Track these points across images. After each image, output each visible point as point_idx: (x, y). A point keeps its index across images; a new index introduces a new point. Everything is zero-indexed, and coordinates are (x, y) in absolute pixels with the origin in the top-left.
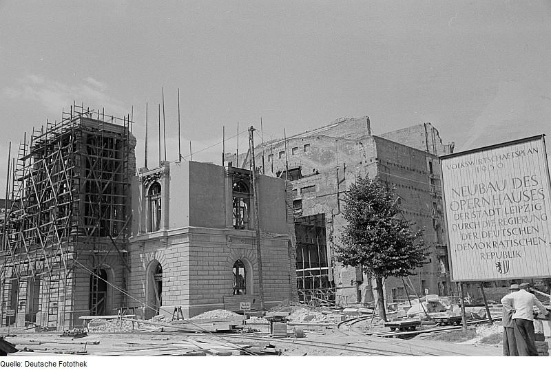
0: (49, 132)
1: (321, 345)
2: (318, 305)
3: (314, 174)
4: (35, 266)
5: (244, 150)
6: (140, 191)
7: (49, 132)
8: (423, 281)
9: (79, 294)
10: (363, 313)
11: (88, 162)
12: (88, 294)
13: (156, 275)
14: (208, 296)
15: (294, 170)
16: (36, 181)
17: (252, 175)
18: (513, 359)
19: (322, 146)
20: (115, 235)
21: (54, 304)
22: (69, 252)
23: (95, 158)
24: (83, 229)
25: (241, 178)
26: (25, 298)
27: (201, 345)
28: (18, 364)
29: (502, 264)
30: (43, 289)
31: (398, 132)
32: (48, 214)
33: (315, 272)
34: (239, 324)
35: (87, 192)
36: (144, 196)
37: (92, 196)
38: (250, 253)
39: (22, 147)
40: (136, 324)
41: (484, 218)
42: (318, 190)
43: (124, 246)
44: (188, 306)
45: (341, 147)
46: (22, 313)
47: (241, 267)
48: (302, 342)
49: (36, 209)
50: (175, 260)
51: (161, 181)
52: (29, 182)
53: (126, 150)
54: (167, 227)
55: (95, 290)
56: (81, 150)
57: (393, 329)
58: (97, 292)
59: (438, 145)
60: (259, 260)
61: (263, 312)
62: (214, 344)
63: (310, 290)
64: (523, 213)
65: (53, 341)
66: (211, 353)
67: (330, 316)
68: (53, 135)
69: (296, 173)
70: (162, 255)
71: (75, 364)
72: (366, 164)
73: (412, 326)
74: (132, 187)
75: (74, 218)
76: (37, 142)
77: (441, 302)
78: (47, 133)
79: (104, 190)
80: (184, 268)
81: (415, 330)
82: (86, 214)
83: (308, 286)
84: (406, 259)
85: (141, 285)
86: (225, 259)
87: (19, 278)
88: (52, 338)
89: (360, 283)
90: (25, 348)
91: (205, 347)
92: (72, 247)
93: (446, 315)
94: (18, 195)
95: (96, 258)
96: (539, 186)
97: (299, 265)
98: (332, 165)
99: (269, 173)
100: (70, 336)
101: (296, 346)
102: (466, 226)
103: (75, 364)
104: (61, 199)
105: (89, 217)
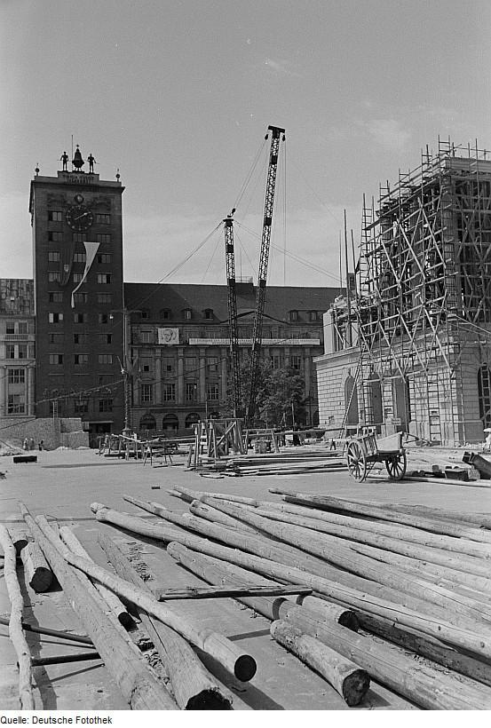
11: (459, 221)
12: (477, 398)
28: (23, 721)
68: (408, 190)
71: (96, 720)
76: (385, 203)
79: (486, 257)
103: (96, 720)
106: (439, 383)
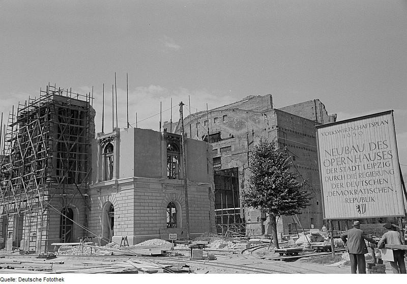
0: (30, 106)
1: (224, 265)
2: (231, 235)
3: (230, 138)
4: (20, 206)
5: (176, 118)
6: (98, 150)
7: (30, 106)
8: (311, 219)
9: (51, 226)
10: (264, 242)
12: (59, 226)
13: (109, 213)
14: (148, 229)
15: (215, 134)
16: (22, 142)
17: (181, 139)
18: (359, 276)
19: (237, 117)
20: (79, 183)
21: (34, 234)
22: (45, 195)
23: (64, 125)
24: (55, 178)
25: (173, 140)
26: (12, 229)
27: (136, 265)
28: (13, 280)
29: (361, 207)
30: (26, 223)
31: (295, 106)
32: (29, 166)
33: (232, 211)
34: (169, 250)
35: (59, 150)
36: (101, 154)
37: (62, 154)
38: (179, 196)
39: (11, 117)
40: (93, 250)
41: (348, 172)
42: (233, 149)
43: (86, 191)
44: (133, 236)
45: (250, 118)
46: (10, 241)
47: (174, 207)
48: (213, 264)
49: (20, 163)
50: (123, 202)
51: (114, 143)
52: (15, 143)
53: (88, 119)
54: (118, 177)
55: (64, 224)
56: (54, 119)
57: (281, 254)
58: (65, 225)
59: (325, 116)
60: (187, 202)
61: (189, 241)
62: (145, 264)
63: (226, 225)
64: (376, 169)
65: (30, 261)
66: (143, 271)
67: (238, 244)
68: (33, 108)
69: (217, 137)
70: (115, 198)
71: (55, 279)
72: (269, 130)
73: (296, 252)
74: (92, 147)
75: (49, 170)
76: (21, 113)
77: (321, 234)
78: (29, 106)
79: (71, 149)
80: (130, 208)
81: (297, 255)
82: (58, 167)
83: (225, 222)
84: (295, 202)
85: (99, 221)
86: (160, 201)
87: (8, 215)
88: (32, 260)
89: (264, 219)
90: (8, 267)
91: (138, 266)
92: (47, 192)
93: (323, 244)
94: (8, 153)
95: (65, 200)
96: (389, 149)
97: (217, 206)
98: (244, 130)
99: (195, 138)
100: (43, 258)
101: (206, 266)
102: (335, 178)
103: (55, 279)
104: (39, 156)
105: (60, 169)
106: (39, 217)
